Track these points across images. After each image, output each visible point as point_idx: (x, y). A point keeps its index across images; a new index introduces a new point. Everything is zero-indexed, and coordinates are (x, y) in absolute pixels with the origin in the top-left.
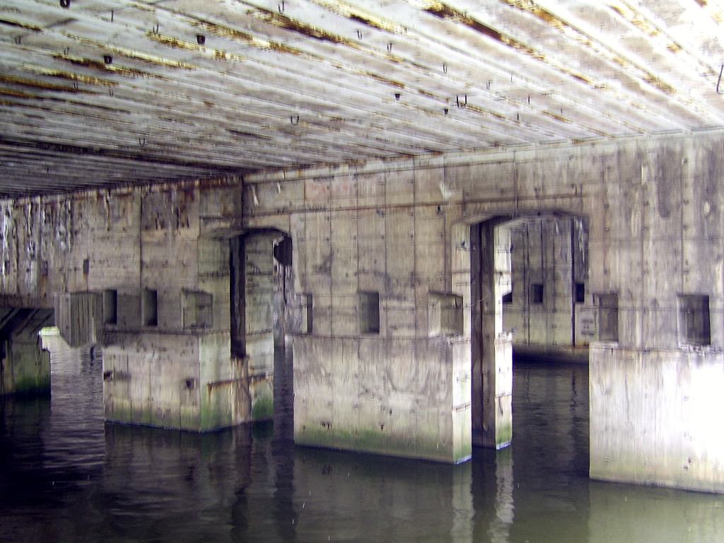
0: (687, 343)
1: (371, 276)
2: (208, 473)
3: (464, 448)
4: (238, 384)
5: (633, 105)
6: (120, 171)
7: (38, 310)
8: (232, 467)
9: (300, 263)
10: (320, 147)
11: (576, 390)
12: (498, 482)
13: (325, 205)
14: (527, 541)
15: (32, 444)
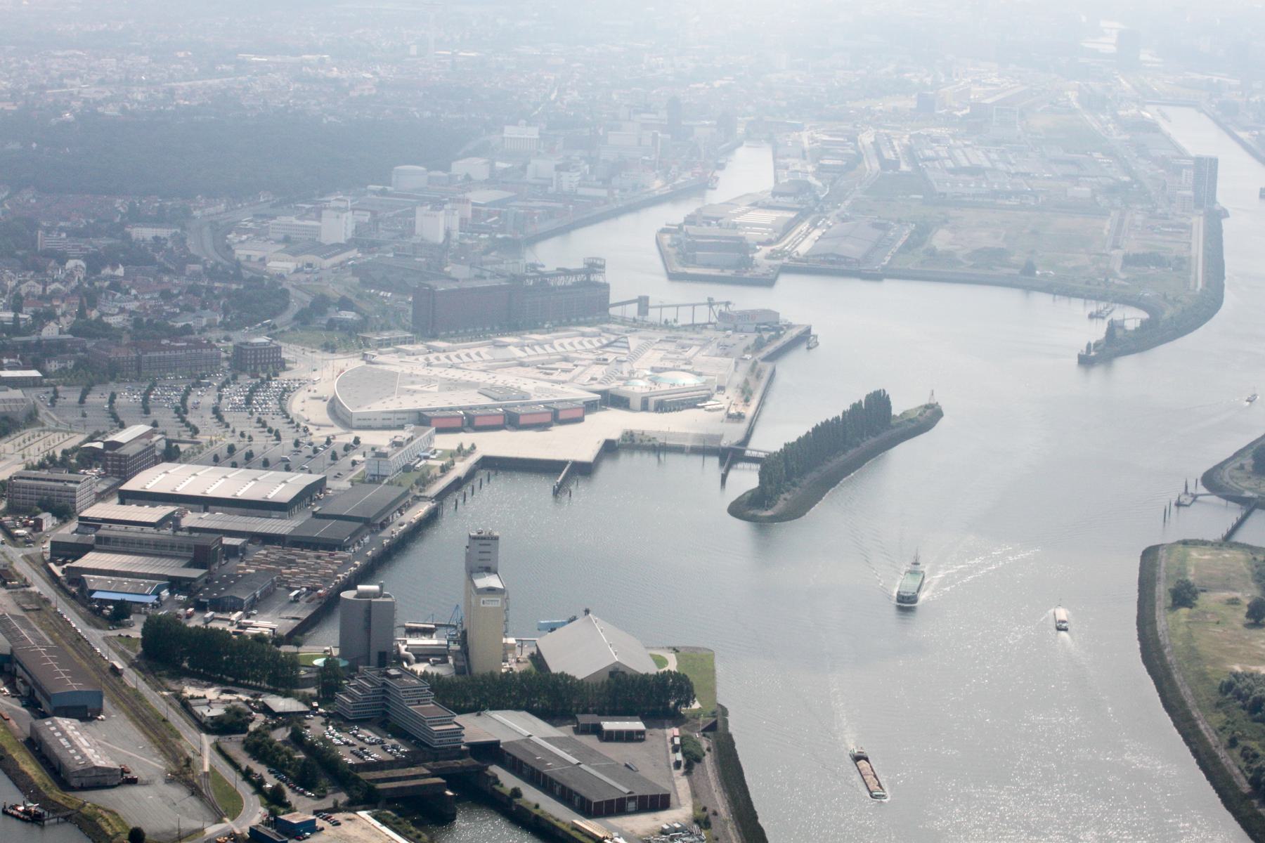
0: (159, 754)
1: (155, 414)
2: (45, 595)
3: (40, 778)
4: (788, 195)
5: (435, 216)
6: (696, 342)
7: (160, 797)
8: (226, 364)
9: (43, 639)
10: (842, 260)
11: (784, 280)
12: (541, 815)
13: (142, 444)
14: (25, 3)
15: (1095, 180)
